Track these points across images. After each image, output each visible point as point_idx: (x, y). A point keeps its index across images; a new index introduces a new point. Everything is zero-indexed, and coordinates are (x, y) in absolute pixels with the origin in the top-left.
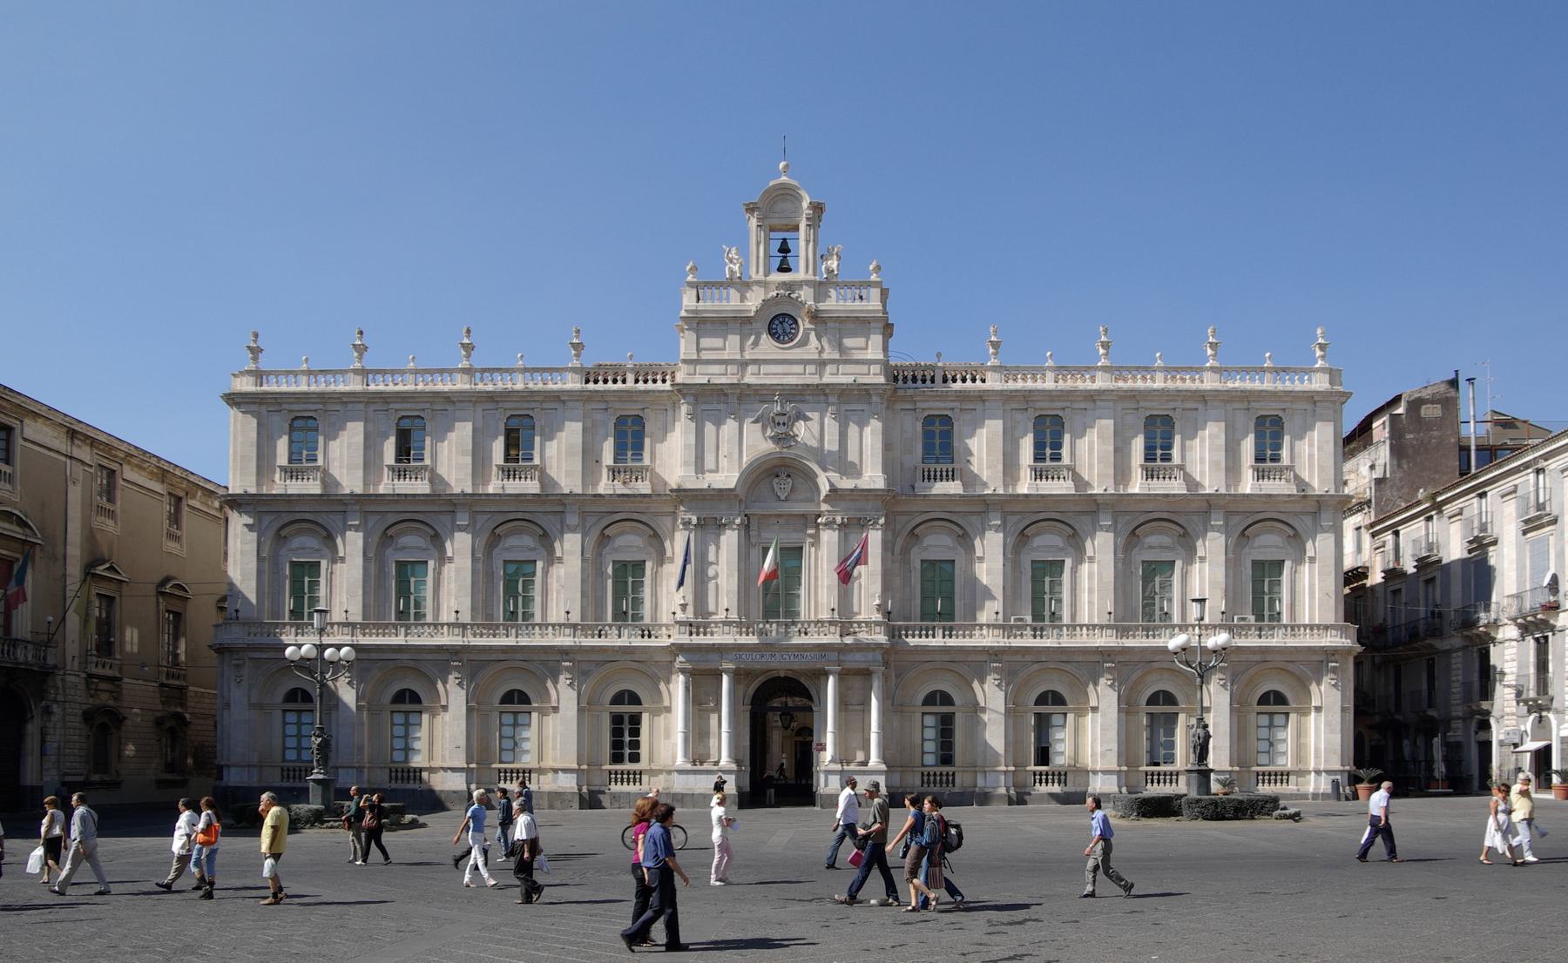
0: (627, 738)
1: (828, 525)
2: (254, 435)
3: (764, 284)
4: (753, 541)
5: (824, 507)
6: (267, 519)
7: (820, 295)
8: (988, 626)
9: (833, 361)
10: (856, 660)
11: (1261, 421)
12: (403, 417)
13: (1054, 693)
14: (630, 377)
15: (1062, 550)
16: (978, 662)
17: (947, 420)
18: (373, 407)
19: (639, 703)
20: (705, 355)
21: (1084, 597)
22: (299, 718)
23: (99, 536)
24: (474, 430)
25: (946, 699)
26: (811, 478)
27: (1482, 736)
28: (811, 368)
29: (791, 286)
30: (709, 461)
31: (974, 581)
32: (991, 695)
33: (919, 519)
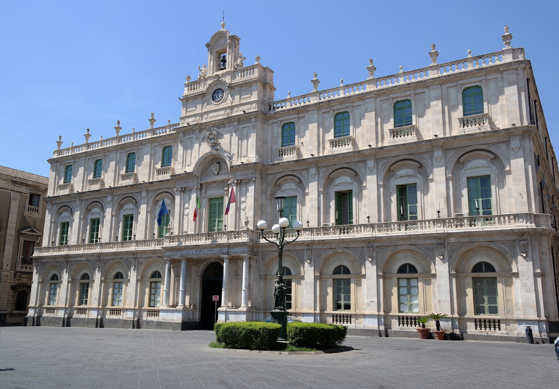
4: (203, 195)
12: (397, 102)
15: (350, 184)
19: (291, 274)
23: (28, 219)
33: (278, 176)
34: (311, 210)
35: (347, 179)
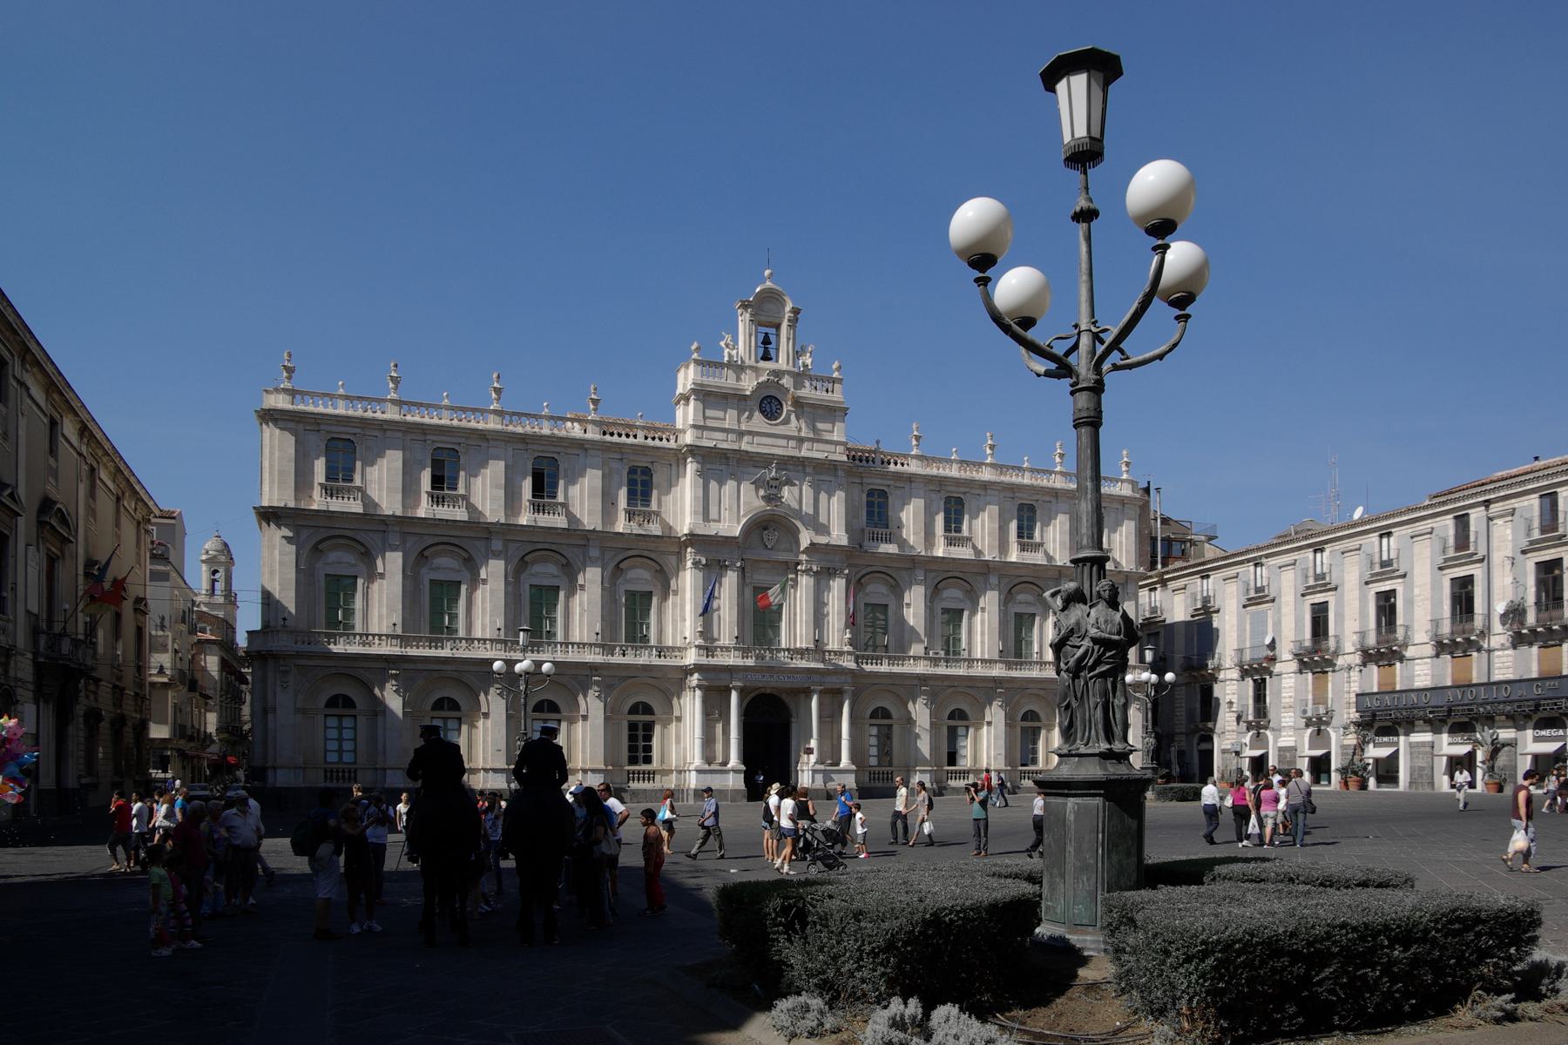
0: (642, 744)
1: (807, 572)
2: (292, 451)
3: (755, 369)
5: (803, 557)
6: (305, 533)
7: (798, 385)
8: (491, 641)
9: (809, 439)
10: (833, 682)
11: (948, 500)
13: (450, 700)
14: (641, 434)
16: (912, 686)
17: (883, 494)
18: (410, 437)
19: (1039, 720)
20: (710, 423)
21: (978, 638)
22: (340, 723)
24: (506, 467)
25: (886, 714)
26: (794, 534)
27: (1204, 746)
28: (792, 443)
29: (778, 374)
30: (713, 514)
31: (902, 621)
32: (920, 712)
33: (430, 541)
34: (484, 610)
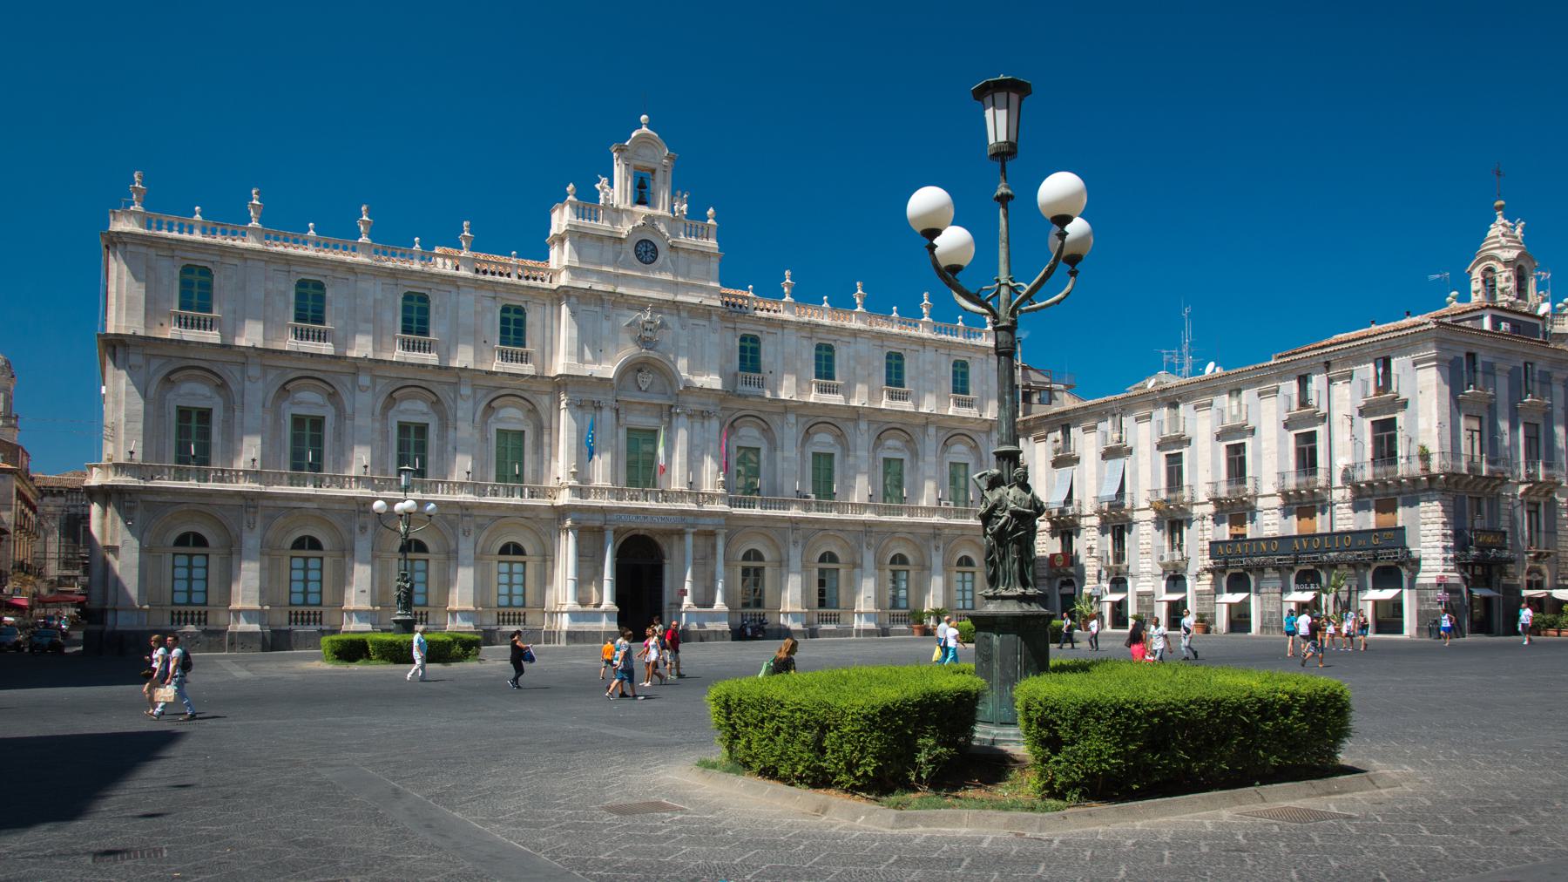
4: (622, 421)
10: (707, 525)
35: (421, 406)
